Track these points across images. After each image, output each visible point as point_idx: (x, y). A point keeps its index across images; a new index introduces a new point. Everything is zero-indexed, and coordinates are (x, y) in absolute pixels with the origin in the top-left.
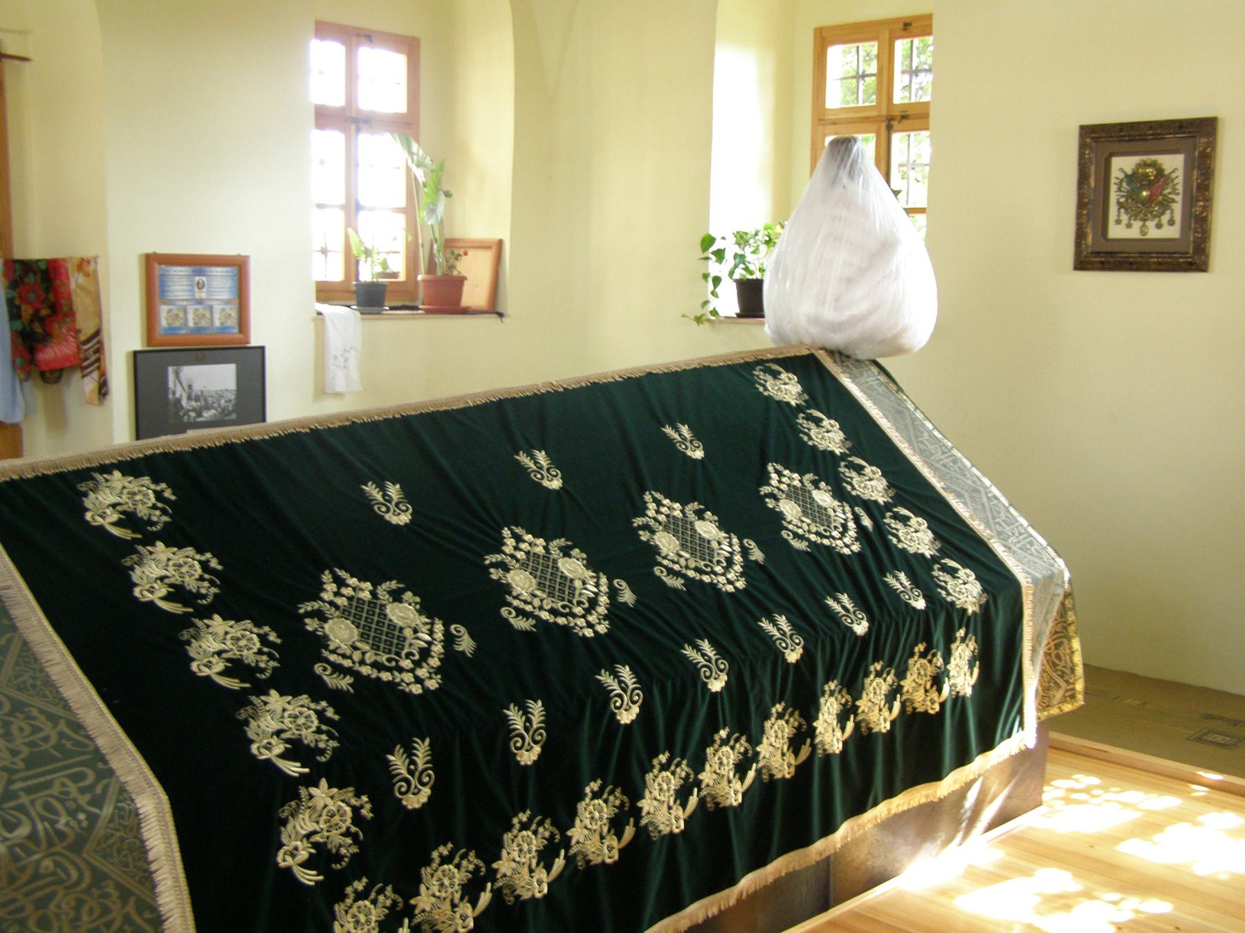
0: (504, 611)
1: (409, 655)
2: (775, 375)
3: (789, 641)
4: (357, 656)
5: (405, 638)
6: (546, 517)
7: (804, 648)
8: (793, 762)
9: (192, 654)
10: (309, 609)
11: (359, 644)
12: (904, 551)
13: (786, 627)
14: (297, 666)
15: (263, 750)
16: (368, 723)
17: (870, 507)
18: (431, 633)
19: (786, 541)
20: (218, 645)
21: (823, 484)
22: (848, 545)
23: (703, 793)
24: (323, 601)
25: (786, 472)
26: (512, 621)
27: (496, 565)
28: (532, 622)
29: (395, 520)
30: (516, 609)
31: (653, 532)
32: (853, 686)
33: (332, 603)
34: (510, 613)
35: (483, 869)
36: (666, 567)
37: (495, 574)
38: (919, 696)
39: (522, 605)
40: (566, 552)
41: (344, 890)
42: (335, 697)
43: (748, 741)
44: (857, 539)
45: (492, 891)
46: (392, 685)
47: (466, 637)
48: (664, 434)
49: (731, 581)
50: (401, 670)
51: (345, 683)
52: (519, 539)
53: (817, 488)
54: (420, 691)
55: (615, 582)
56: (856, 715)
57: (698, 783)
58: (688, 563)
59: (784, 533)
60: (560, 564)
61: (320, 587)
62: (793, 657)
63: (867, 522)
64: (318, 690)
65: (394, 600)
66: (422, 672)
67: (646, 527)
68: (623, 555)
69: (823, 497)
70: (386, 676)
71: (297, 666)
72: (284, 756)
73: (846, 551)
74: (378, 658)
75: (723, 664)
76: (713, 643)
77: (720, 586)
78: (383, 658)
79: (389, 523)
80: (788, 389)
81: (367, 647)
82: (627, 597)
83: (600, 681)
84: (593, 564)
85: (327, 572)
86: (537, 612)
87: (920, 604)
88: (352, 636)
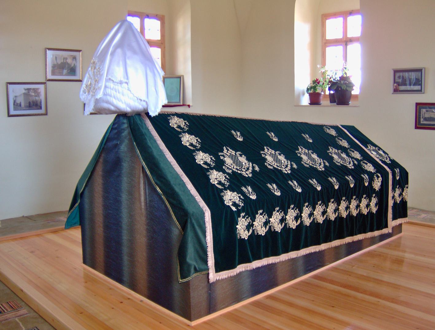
0: (266, 164)
1: (244, 168)
2: (329, 129)
3: (336, 183)
4: (232, 166)
5: (243, 165)
6: (308, 146)
7: (339, 186)
8: (334, 216)
9: (196, 158)
10: (221, 154)
11: (233, 164)
12: (366, 170)
13: (335, 180)
14: (219, 166)
15: (213, 182)
16: (236, 182)
17: (357, 159)
18: (249, 165)
19: (303, 164)
20: (202, 158)
21: (343, 153)
22: (351, 166)
23: (314, 217)
24: (224, 153)
25: (334, 149)
26: (226, 170)
27: (222, 155)
28: (231, 171)
29: (239, 139)
30: (269, 164)
31: (225, 157)
32: (349, 200)
33: (226, 154)
34: (267, 164)
35: (251, 223)
36: (304, 162)
37: (263, 156)
38: (353, 210)
39: (228, 166)
40: (241, 155)
41: (240, 215)
42: (228, 174)
43: (325, 206)
44: (353, 166)
45: (269, 226)
46: (241, 174)
47: (295, 165)
48: (302, 136)
49: (321, 168)
50: (243, 171)
51: (230, 171)
52: (302, 149)
53: (379, 150)
54: (287, 173)
55: (254, 165)
56: (338, 211)
57: (313, 214)
58: (235, 168)
59: (302, 162)
60: (278, 157)
61: (223, 150)
62: (352, 186)
63: (356, 162)
64: (224, 172)
65: (240, 156)
66: (247, 172)
67: (299, 153)
68: (259, 160)
69: (344, 155)
70: (239, 171)
71: (219, 166)
72: (217, 184)
73: (350, 168)
74: (237, 168)
75: (338, 183)
76: (316, 180)
77: (283, 171)
78: (238, 168)
79: (238, 140)
80: (333, 132)
81: (234, 165)
82: (257, 169)
83: (267, 186)
84: (248, 159)
85: (225, 147)
86: (273, 165)
87: (366, 184)
88: (231, 162)
